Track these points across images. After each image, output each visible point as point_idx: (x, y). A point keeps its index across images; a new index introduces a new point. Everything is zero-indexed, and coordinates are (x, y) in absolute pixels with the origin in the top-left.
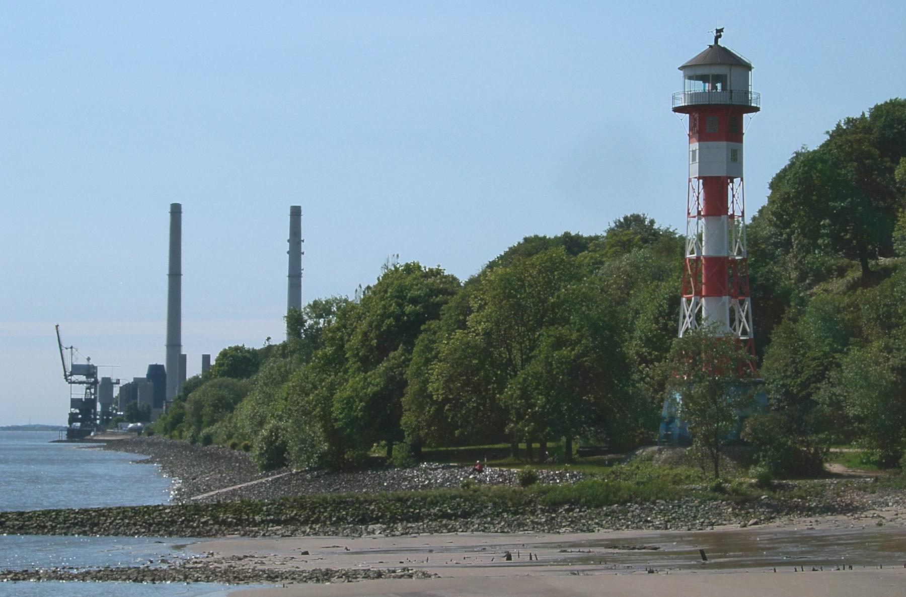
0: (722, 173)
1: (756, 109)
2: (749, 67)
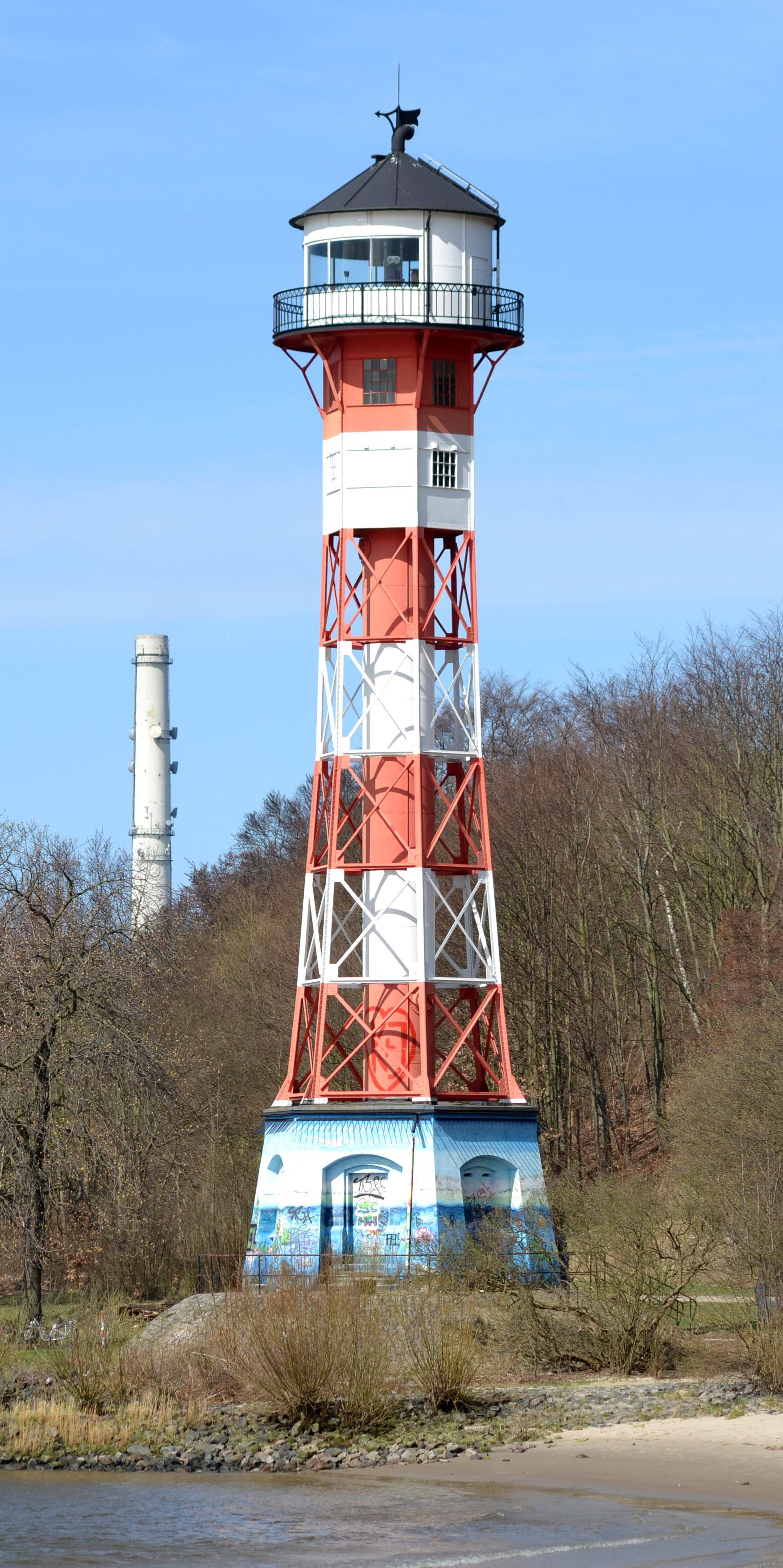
0: (409, 521)
1: (513, 339)
2: (498, 222)
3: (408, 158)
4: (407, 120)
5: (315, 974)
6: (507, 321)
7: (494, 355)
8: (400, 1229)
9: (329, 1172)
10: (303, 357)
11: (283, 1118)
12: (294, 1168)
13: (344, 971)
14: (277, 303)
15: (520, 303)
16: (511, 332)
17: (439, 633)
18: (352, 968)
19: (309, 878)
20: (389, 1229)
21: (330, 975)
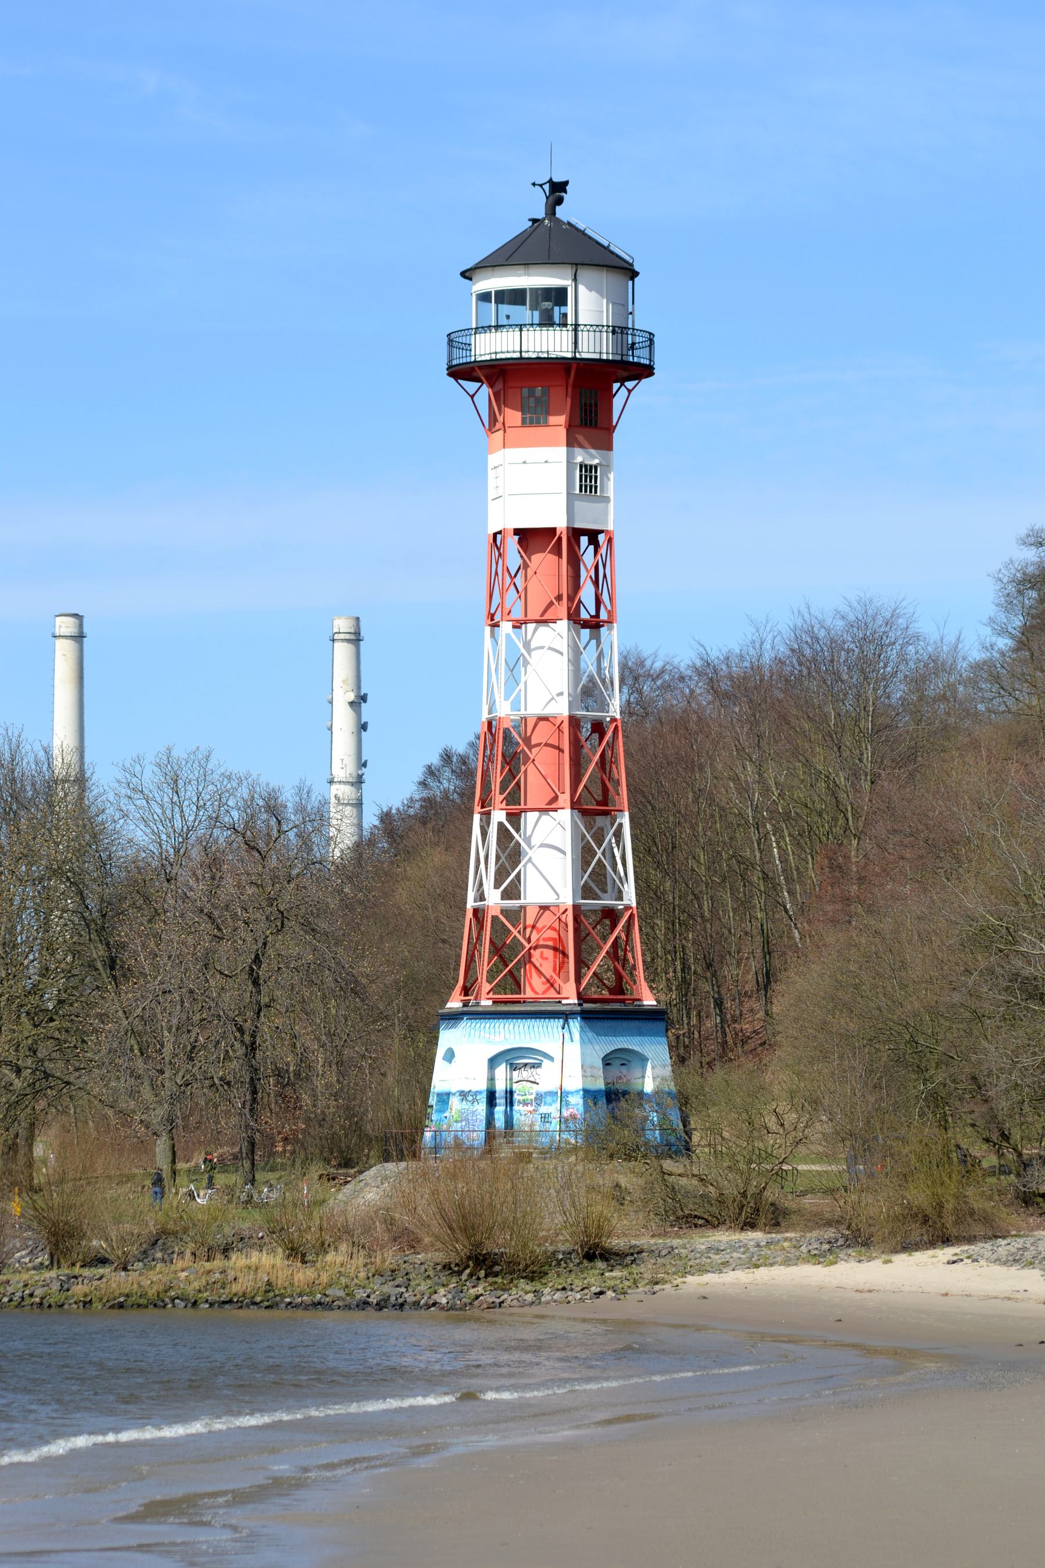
0: (559, 521)
1: (646, 371)
2: (633, 274)
3: (559, 221)
4: (557, 190)
5: (482, 898)
6: (641, 357)
7: (630, 384)
8: (552, 1109)
9: (493, 1062)
10: (471, 386)
11: (455, 1017)
12: (464, 1059)
13: (507, 895)
14: (450, 341)
15: (651, 341)
16: (639, 365)
17: (584, 615)
18: (512, 892)
19: (477, 818)
20: (543, 1109)
21: (494, 898)
